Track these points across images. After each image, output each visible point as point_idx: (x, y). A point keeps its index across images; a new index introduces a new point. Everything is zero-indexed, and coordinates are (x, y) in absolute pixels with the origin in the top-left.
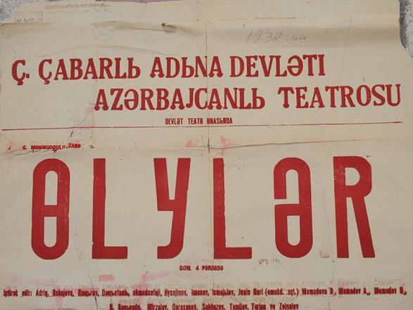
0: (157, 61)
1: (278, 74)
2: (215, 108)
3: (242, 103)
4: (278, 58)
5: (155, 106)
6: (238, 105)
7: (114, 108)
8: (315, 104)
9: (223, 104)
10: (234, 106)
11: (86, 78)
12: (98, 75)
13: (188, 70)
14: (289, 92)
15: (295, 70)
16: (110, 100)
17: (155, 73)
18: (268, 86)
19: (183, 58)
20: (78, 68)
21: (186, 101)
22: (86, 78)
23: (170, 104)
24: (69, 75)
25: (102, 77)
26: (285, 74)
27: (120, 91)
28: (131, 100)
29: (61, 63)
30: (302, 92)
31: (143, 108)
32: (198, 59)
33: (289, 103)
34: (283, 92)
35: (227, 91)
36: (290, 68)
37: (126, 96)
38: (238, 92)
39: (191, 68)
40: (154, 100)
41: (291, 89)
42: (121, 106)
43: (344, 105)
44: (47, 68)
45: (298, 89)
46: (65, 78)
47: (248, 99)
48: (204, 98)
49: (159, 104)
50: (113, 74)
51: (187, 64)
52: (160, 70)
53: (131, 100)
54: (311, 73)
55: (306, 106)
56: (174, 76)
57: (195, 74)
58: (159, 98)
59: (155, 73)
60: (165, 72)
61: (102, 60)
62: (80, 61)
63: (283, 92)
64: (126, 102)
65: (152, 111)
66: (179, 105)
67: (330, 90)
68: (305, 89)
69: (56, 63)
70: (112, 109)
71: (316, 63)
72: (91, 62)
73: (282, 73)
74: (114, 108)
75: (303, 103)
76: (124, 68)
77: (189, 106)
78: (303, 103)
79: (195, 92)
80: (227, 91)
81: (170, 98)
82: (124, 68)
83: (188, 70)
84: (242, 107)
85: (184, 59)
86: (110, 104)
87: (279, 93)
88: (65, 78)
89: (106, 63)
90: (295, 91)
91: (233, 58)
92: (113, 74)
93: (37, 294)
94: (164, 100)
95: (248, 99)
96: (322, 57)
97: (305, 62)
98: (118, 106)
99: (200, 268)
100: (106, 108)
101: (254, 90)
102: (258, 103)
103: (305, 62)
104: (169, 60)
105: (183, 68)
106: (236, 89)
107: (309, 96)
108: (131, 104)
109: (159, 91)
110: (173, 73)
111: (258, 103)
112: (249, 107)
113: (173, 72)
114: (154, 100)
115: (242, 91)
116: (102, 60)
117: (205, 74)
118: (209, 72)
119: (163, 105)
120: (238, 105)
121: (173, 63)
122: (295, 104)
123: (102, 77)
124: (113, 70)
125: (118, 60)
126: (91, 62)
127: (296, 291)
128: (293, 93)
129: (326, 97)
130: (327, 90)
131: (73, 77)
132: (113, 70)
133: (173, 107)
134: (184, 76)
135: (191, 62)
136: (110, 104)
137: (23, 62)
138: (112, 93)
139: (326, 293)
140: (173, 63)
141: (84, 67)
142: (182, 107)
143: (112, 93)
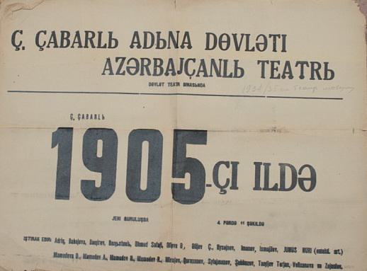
0: (136, 34)
1: (247, 50)
2: (287, 78)
3: (225, 73)
4: (248, 36)
5: (323, 76)
6: (222, 74)
7: (118, 73)
8: (200, 74)
9: (209, 74)
10: (218, 75)
11: (73, 47)
12: (83, 44)
13: (161, 42)
14: (305, 65)
15: (262, 47)
16: (115, 66)
17: (134, 44)
18: (249, 61)
19: (157, 32)
20: (67, 39)
21: (177, 68)
22: (73, 47)
23: (165, 72)
24: (59, 44)
25: (86, 46)
26: (253, 50)
27: (124, 59)
28: (132, 67)
29: (53, 34)
30: (276, 65)
31: (142, 74)
32: (171, 34)
33: (304, 75)
34: (299, 65)
35: (213, 61)
36: (257, 45)
37: (128, 63)
38: (223, 62)
39: (164, 41)
40: (151, 68)
41: (307, 63)
42: (124, 72)
43: (312, 78)
44: (42, 38)
45: (273, 62)
46: (56, 46)
47: (231, 69)
48: (192, 67)
49: (155, 70)
50: (96, 45)
51: (161, 38)
52: (138, 42)
53: (132, 67)
54: (275, 50)
55: (278, 77)
56: (213, 49)
57: (167, 46)
58: (155, 65)
59: (134, 44)
60: (142, 44)
61: (87, 32)
62: (68, 33)
63: (299, 65)
64: (128, 69)
65: (219, 78)
66: (289, 75)
67: (261, 63)
68: (279, 62)
69: (49, 34)
70: (117, 74)
71: (279, 41)
72: (78, 34)
73: (250, 49)
74: (118, 73)
75: (276, 74)
76: (105, 40)
77: (179, 72)
78: (276, 75)
79: (184, 61)
80: (213, 61)
81: (165, 66)
82: (105, 40)
83: (161, 42)
84: (225, 76)
85: (159, 33)
86: (115, 71)
87: (296, 66)
88: (56, 46)
89: (90, 35)
90: (310, 64)
91: (208, 34)
92: (96, 45)
93: (56, 242)
94: (141, 67)
95: (231, 69)
96: (284, 36)
97: (270, 41)
98: (121, 72)
99: (222, 222)
100: (111, 73)
101: (236, 62)
102: (239, 72)
103: (270, 41)
104: (146, 33)
105: (157, 41)
106: (220, 60)
107: (281, 68)
108: (133, 71)
109: (155, 60)
110: (148, 45)
111: (239, 72)
112: (231, 76)
113: (149, 44)
114: (151, 68)
115: (226, 61)
116: (87, 32)
117: (177, 47)
118: (180, 44)
119: (158, 72)
120: (222, 74)
121: (149, 36)
122: (270, 76)
123: (86, 46)
124: (95, 40)
125: (100, 33)
126: (78, 34)
127: (340, 252)
128: (308, 66)
129: (296, 71)
130: (258, 63)
131: (62, 46)
132: (95, 40)
133: (167, 74)
134: (158, 48)
135: (165, 36)
136: (115, 71)
137: (21, 32)
138: (117, 61)
139: (125, 218)
140: (149, 36)
141: (71, 39)
142: (174, 74)
143: (117, 61)
